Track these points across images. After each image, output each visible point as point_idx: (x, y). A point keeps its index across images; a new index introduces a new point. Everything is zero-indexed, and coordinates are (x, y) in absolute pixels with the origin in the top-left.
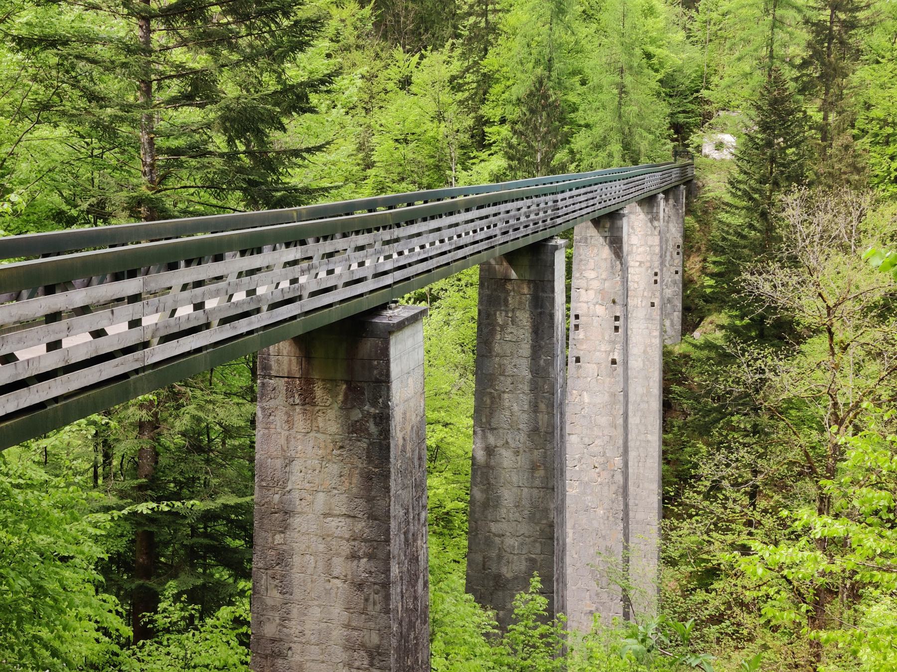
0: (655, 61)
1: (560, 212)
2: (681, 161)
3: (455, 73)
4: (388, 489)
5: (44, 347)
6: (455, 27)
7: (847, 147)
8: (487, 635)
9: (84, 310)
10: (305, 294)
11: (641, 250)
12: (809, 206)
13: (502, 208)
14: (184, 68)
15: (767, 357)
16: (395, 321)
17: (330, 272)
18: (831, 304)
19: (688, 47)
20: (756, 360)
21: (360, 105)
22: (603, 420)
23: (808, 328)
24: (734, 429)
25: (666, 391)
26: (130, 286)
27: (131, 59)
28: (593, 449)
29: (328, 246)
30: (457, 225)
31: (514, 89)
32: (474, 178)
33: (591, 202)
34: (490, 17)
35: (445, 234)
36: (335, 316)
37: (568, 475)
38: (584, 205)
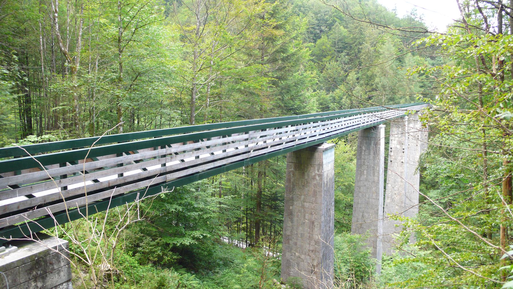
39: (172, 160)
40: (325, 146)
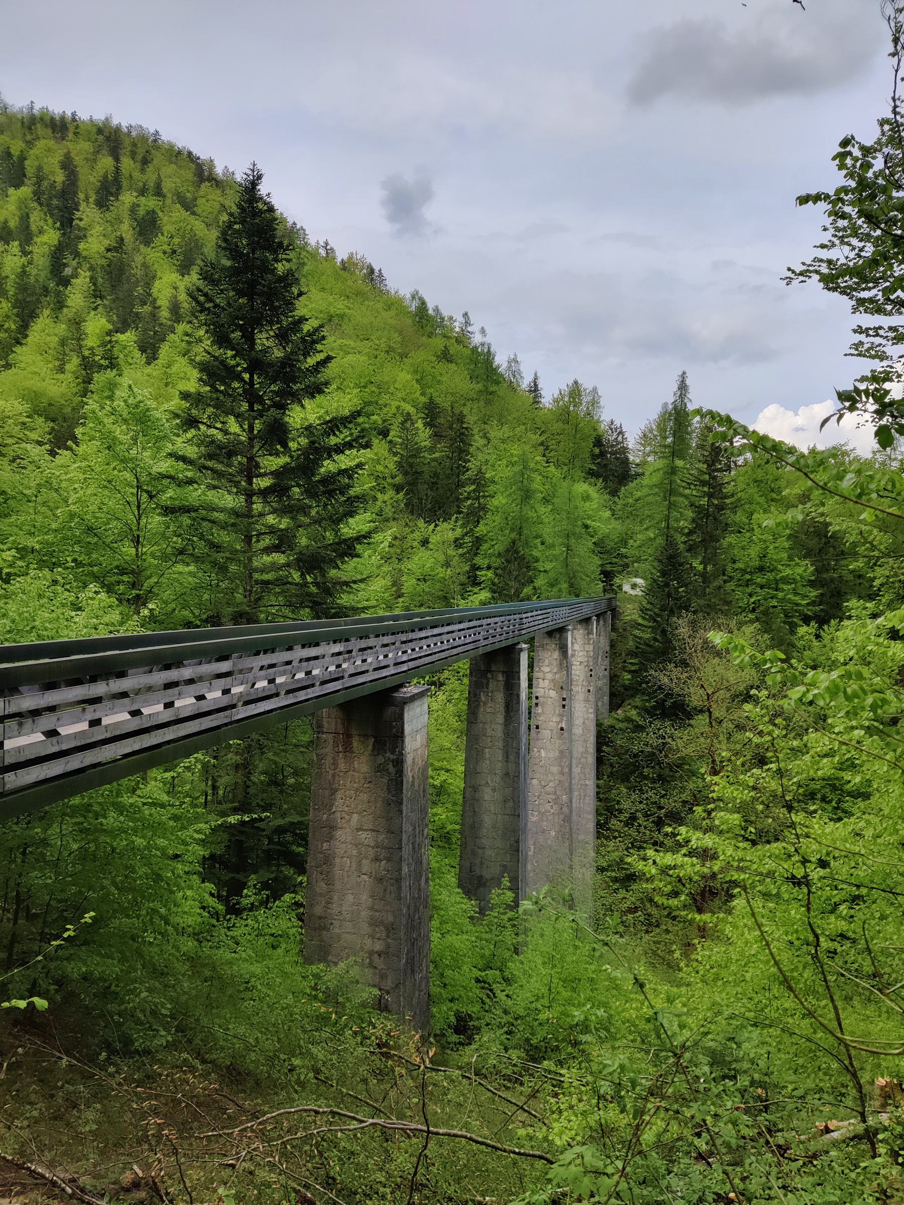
0: (590, 530)
1: (525, 626)
2: (608, 596)
3: (457, 536)
4: (401, 812)
5: (162, 706)
6: (459, 507)
7: (720, 587)
8: (471, 918)
9: (191, 681)
10: (346, 675)
11: (581, 654)
12: (693, 624)
13: (485, 622)
14: (274, 528)
15: (667, 727)
16: (408, 695)
17: (364, 661)
18: (710, 692)
19: (613, 521)
20: (659, 729)
21: (394, 556)
22: (555, 769)
23: (695, 708)
24: (646, 778)
25: (599, 750)
26: (224, 667)
27: (238, 521)
28: (548, 789)
29: (363, 644)
30: (453, 632)
31: (496, 547)
32: (469, 604)
33: (546, 620)
34: (482, 501)
35: (445, 638)
36: (366, 691)
37: (530, 807)
38: (541, 622)
39: (23, 731)
40: (411, 690)
